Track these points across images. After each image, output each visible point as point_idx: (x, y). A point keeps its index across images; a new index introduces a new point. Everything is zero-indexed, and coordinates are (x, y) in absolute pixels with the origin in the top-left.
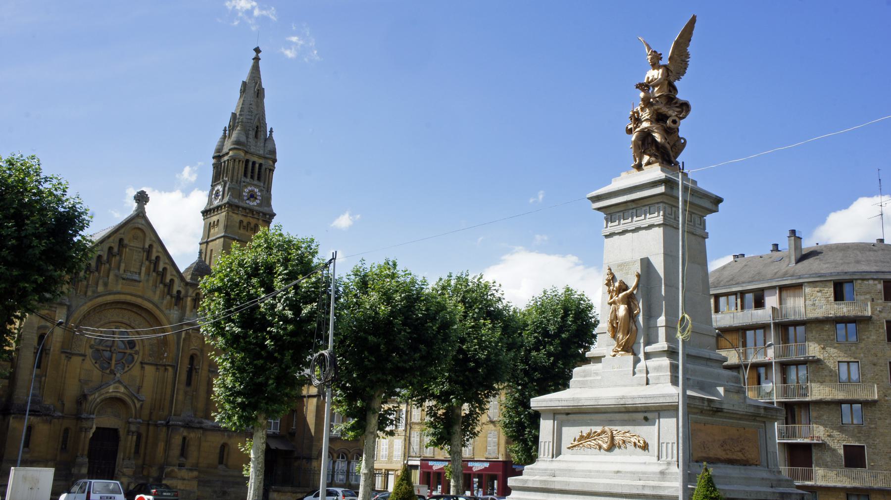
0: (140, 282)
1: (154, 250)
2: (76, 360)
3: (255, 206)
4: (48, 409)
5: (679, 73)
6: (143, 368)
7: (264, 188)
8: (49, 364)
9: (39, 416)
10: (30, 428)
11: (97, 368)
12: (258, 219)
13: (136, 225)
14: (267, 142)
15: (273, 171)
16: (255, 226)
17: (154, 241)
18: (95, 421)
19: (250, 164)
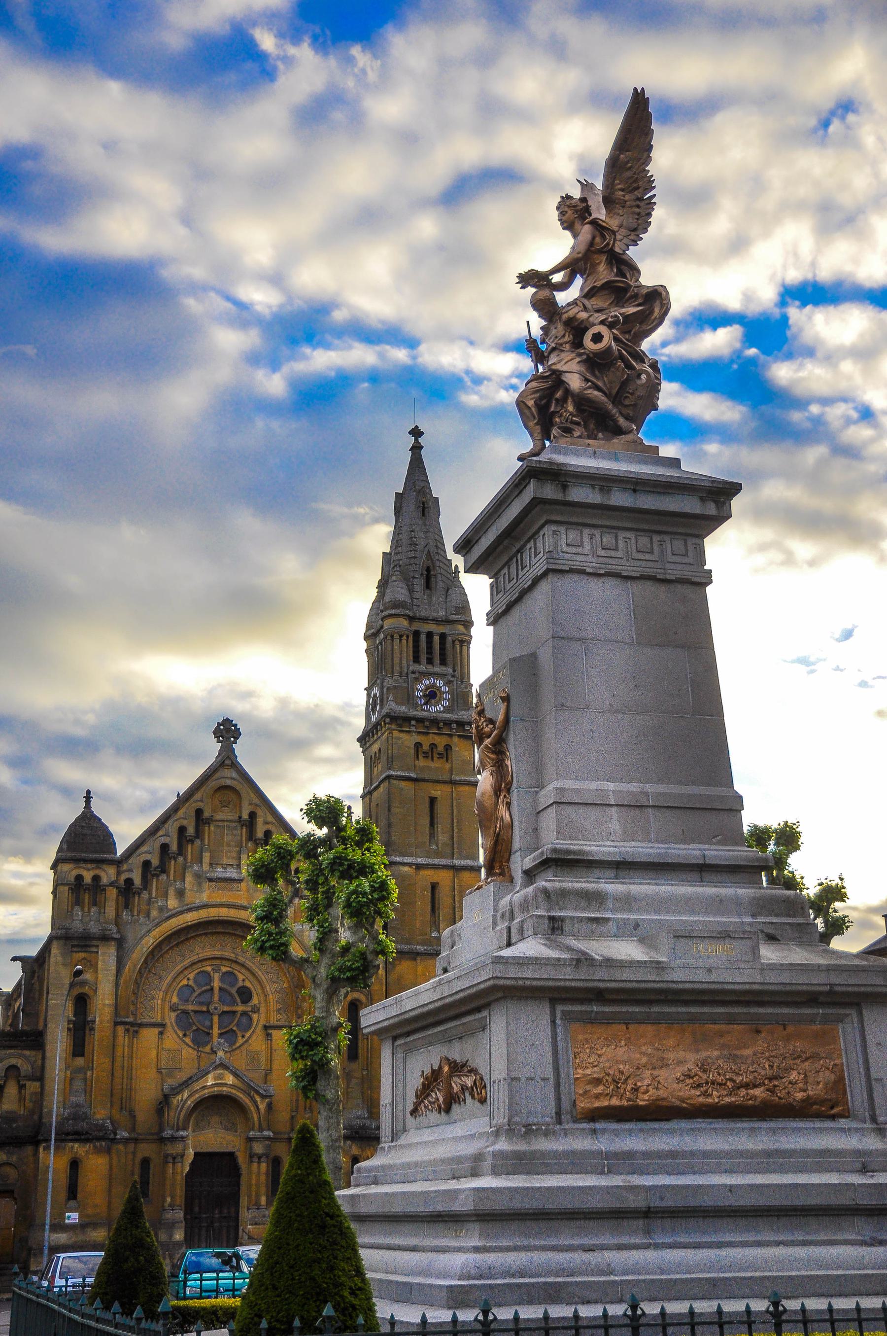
0: (240, 881)
1: (260, 821)
2: (149, 1035)
3: (441, 712)
4: (102, 1127)
5: (635, 230)
6: (268, 1036)
7: (453, 676)
8: (95, 1048)
9: (87, 1140)
10: (75, 1164)
11: (187, 1044)
12: (451, 736)
13: (223, 782)
14: (450, 592)
15: (469, 643)
16: (447, 750)
17: (257, 805)
18: (190, 1142)
19: (423, 638)
